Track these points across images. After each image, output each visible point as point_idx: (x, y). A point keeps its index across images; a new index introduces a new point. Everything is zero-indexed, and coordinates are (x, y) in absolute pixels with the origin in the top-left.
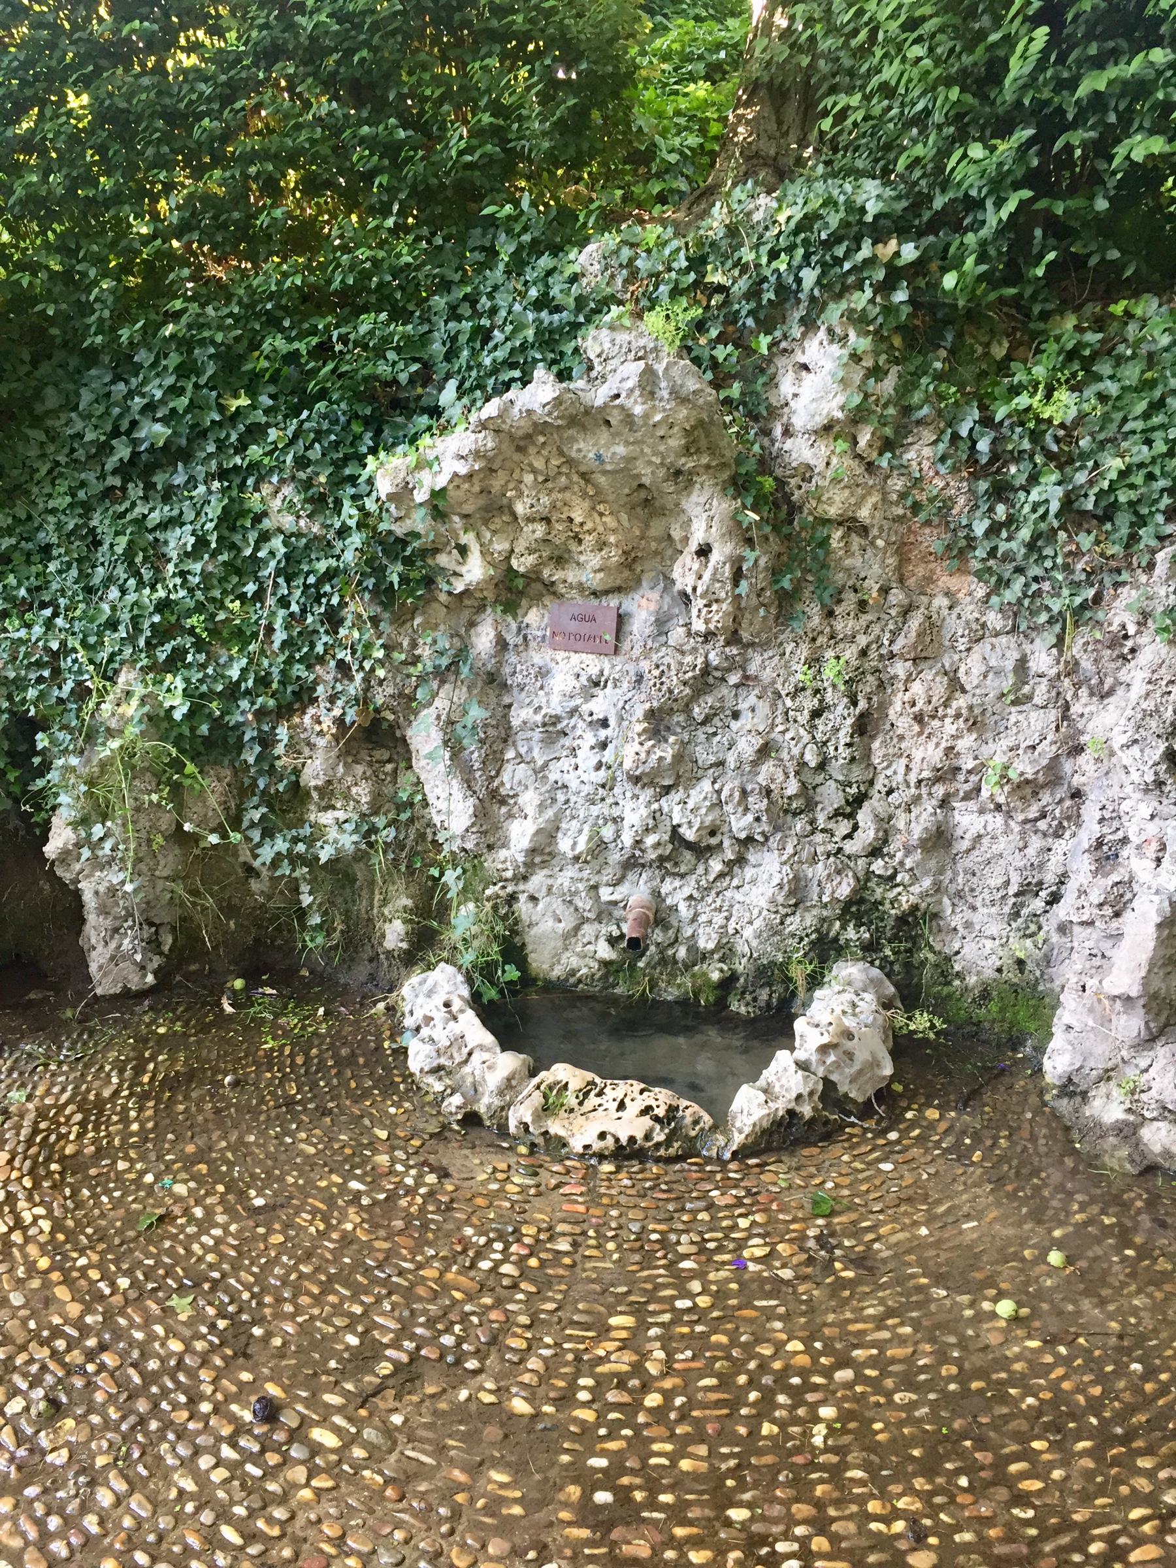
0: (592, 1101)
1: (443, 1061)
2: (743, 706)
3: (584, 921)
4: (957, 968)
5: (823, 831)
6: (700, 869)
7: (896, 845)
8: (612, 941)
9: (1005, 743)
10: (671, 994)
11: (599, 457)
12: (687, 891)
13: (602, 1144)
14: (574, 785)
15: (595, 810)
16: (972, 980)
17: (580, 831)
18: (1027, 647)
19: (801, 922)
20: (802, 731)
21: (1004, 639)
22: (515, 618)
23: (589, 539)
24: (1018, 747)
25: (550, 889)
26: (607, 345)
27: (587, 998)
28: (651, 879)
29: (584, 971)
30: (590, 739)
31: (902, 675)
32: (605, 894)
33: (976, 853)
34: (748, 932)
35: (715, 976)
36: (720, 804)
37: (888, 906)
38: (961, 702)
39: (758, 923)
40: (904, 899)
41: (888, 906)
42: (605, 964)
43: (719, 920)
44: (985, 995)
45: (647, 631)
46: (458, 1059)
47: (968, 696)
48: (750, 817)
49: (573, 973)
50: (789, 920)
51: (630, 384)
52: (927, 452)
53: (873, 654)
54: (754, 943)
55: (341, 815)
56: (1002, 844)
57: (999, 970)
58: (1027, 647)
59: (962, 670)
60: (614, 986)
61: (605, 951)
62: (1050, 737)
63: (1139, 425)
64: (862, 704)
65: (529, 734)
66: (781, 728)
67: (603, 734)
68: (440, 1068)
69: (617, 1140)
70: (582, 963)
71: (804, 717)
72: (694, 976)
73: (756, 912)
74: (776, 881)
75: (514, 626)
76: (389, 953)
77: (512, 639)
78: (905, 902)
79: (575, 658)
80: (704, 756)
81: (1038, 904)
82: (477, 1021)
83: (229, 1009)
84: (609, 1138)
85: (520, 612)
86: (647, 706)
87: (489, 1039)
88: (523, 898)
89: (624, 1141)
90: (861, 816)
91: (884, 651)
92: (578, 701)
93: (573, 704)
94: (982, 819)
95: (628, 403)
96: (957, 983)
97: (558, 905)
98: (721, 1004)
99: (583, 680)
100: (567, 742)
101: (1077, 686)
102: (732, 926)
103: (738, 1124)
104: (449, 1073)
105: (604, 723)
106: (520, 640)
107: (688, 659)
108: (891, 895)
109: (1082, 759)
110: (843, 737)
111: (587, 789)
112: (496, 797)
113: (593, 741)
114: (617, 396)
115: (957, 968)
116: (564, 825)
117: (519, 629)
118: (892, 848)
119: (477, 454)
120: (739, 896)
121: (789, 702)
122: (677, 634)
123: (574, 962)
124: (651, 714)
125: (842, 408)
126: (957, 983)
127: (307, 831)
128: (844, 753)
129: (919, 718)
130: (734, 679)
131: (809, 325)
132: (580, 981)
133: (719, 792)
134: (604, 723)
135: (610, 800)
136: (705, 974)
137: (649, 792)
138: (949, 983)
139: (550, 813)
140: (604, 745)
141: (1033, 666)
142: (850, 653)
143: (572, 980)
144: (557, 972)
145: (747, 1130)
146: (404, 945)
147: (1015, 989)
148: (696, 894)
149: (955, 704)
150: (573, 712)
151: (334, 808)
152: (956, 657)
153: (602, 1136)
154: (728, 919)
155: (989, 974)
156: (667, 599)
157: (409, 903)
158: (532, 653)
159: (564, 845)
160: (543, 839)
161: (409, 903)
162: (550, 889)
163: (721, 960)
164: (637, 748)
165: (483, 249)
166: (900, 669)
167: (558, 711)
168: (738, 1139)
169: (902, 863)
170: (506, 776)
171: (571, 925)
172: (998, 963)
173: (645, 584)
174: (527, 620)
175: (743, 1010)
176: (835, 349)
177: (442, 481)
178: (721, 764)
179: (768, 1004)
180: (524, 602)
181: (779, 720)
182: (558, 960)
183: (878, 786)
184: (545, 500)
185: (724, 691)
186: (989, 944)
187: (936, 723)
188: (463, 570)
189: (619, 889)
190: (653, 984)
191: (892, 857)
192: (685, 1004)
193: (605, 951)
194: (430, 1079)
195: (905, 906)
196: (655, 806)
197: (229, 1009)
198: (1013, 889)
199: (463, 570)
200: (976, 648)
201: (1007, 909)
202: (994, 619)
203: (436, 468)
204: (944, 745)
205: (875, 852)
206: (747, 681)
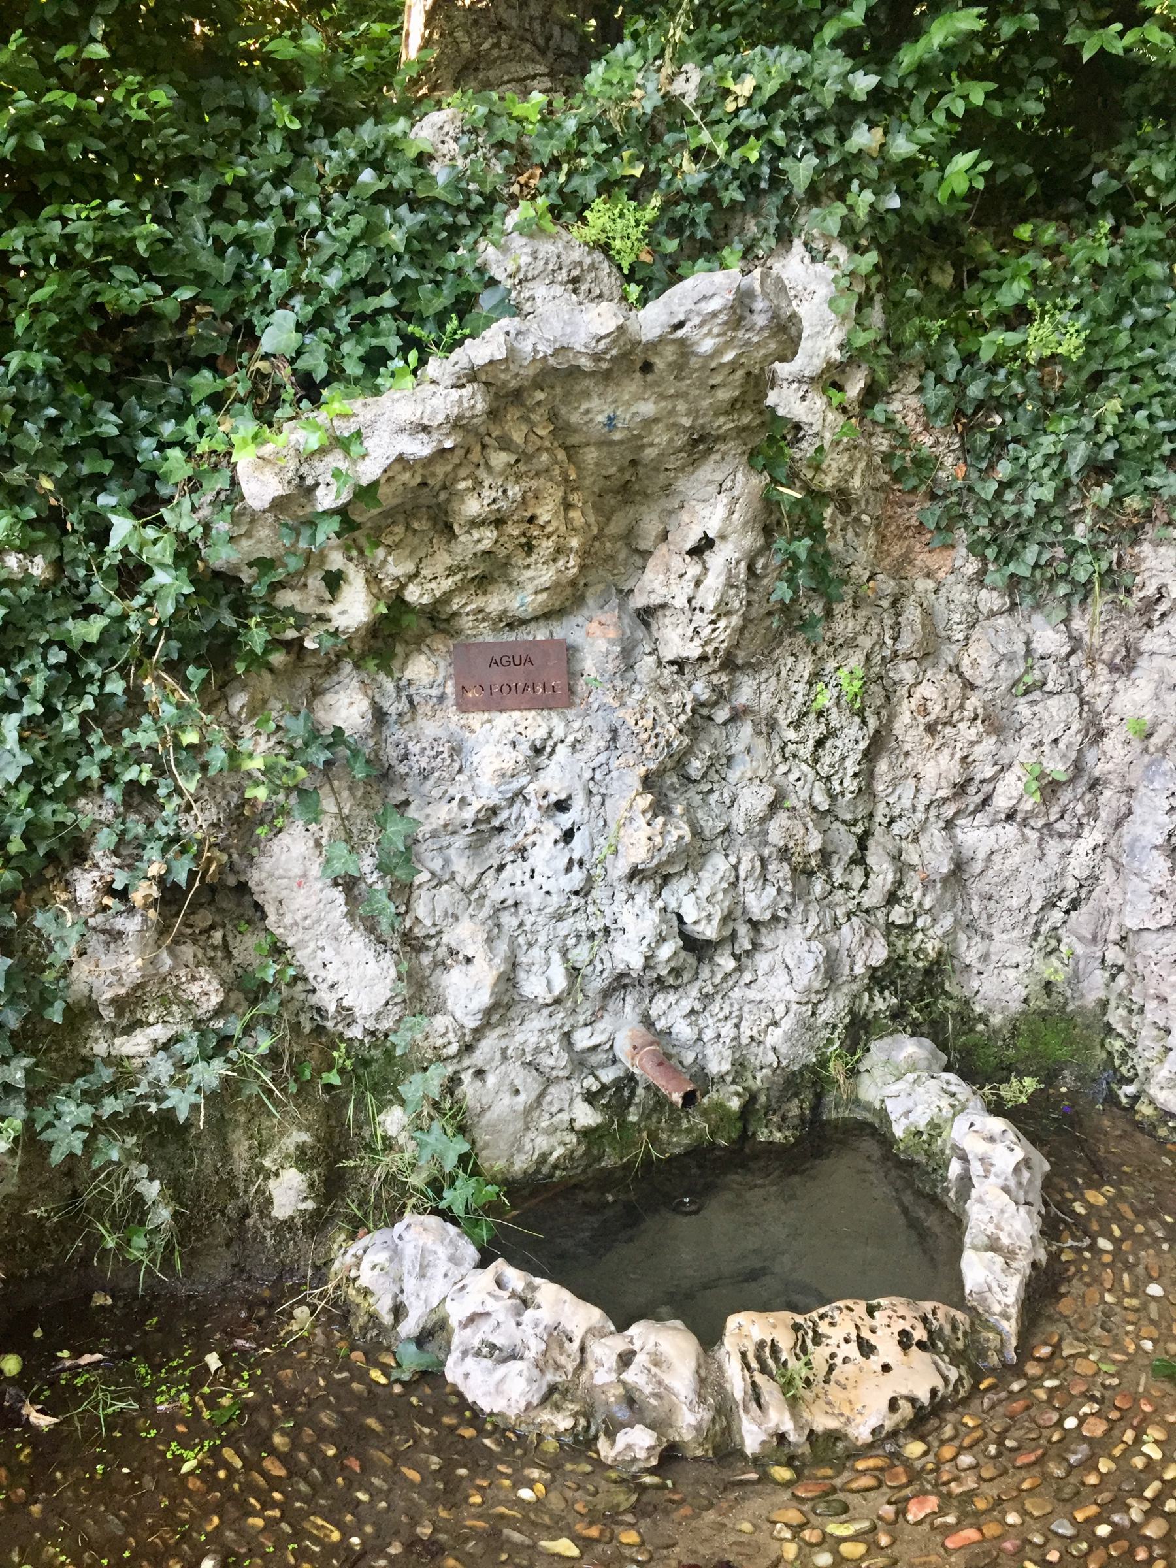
0: (819, 1355)
1: (551, 1377)
2: (738, 747)
3: (549, 1082)
4: (978, 1009)
5: (841, 886)
6: (705, 972)
7: (912, 887)
8: (591, 1098)
9: (1026, 742)
10: (678, 1143)
11: (611, 421)
12: (686, 1005)
13: (897, 1417)
14: (536, 900)
15: (564, 928)
16: (996, 1020)
17: (548, 963)
18: (1027, 627)
19: (833, 1009)
20: (804, 767)
21: (1001, 621)
22: (389, 673)
23: (546, 546)
24: (1041, 743)
25: (504, 1051)
26: (524, 260)
27: (571, 1188)
28: (639, 1001)
29: (559, 1152)
30: (552, 830)
31: (909, 678)
32: (582, 1039)
33: (991, 872)
34: (775, 1037)
35: (735, 1104)
36: (734, 885)
37: (911, 959)
38: (974, 702)
39: (787, 1024)
40: (929, 946)
41: (911, 959)
42: (587, 1134)
43: (727, 1030)
44: (1015, 1031)
45: (610, 667)
46: (570, 1367)
47: (978, 693)
48: (771, 891)
49: (544, 1158)
50: (821, 1007)
51: (714, 305)
52: (913, 401)
53: (876, 659)
54: (783, 1049)
55: (160, 1033)
56: (1016, 858)
57: (1026, 1001)
58: (1027, 627)
59: (966, 661)
60: (600, 1159)
61: (587, 1117)
62: (1075, 728)
63: (1126, 363)
64: (873, 722)
65: (448, 839)
66: (782, 768)
67: (566, 820)
68: (553, 1389)
69: (912, 1400)
70: (554, 1141)
71: (805, 752)
72: (705, 1113)
73: (780, 1010)
74: (812, 964)
75: (389, 685)
76: (288, 1224)
77: (393, 707)
78: (931, 947)
79: (503, 720)
80: (711, 825)
81: (1056, 916)
82: (566, 1294)
83: (44, 1422)
84: (901, 1402)
85: (396, 664)
86: (642, 770)
87: (593, 1315)
88: (466, 1077)
89: (924, 1397)
90: (871, 860)
91: (887, 653)
92: (524, 780)
93: (515, 785)
94: (992, 833)
95: (696, 335)
96: (980, 1027)
97: (518, 1074)
98: (745, 1136)
99: (524, 749)
100: (507, 840)
101: (1092, 661)
102: (746, 1032)
103: (997, 1308)
104: (565, 1393)
105: (562, 806)
106: (403, 705)
107: (675, 698)
108: (914, 946)
109: (1107, 744)
110: (851, 766)
111: (555, 901)
112: (412, 943)
113: (557, 834)
114: (681, 325)
115: (978, 1009)
116: (523, 959)
117: (398, 689)
118: (908, 889)
119: (457, 424)
120: (752, 994)
121: (791, 734)
122: (646, 665)
123: (543, 1143)
124: (648, 782)
125: (841, 347)
126: (980, 1027)
127: (107, 1074)
128: (851, 785)
129: (930, 729)
130: (722, 714)
131: (784, 237)
132: (555, 1167)
133: (736, 867)
134: (562, 806)
135: (591, 909)
136: (720, 1106)
137: (648, 887)
138: (972, 1030)
139: (502, 947)
140: (568, 836)
141: (1039, 647)
142: (855, 661)
143: (545, 1170)
144: (521, 1164)
145: (1013, 1311)
146: (310, 1205)
147: (1043, 1015)
148: (698, 1006)
149: (969, 705)
150: (519, 795)
151: (140, 1024)
152: (955, 648)
153: (893, 1405)
154: (737, 1026)
155: (1016, 1007)
156: (626, 621)
157: (304, 1137)
158: (421, 721)
159: (533, 986)
160: (503, 986)
161: (304, 1137)
162: (504, 1051)
163: (734, 1082)
164: (648, 831)
165: (233, 111)
166: (905, 671)
167: (496, 799)
168: (1010, 1327)
169: (920, 904)
170: (421, 909)
171: (534, 1095)
172: (1024, 993)
173: (590, 602)
174: (408, 674)
175: (778, 1136)
176: (823, 269)
177: (369, 471)
178: (727, 830)
179: (802, 1117)
180: (399, 649)
181: (778, 758)
182: (517, 1145)
183: (879, 818)
184: (514, 491)
185: (716, 733)
186: (1012, 974)
187: (948, 730)
188: (333, 611)
189: (599, 1026)
190: (653, 1137)
191: (909, 899)
192: (699, 1153)
193: (587, 1117)
194: (545, 1416)
195: (933, 955)
196: (659, 904)
197: (44, 1422)
198: (1036, 906)
199: (333, 611)
200: (976, 633)
201: (1029, 930)
202: (990, 599)
203: (355, 449)
204: (958, 755)
205: (892, 899)
206: (736, 717)
